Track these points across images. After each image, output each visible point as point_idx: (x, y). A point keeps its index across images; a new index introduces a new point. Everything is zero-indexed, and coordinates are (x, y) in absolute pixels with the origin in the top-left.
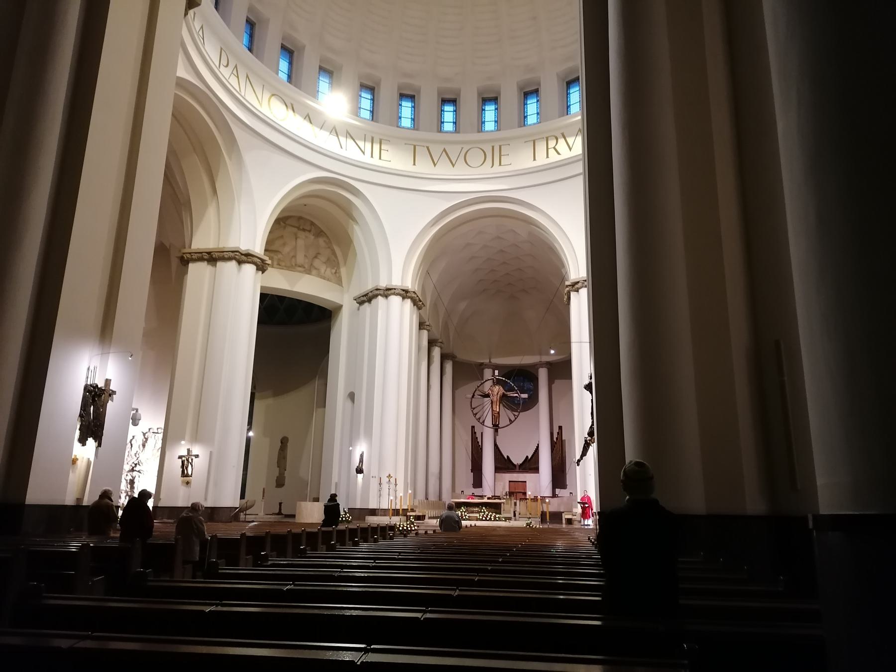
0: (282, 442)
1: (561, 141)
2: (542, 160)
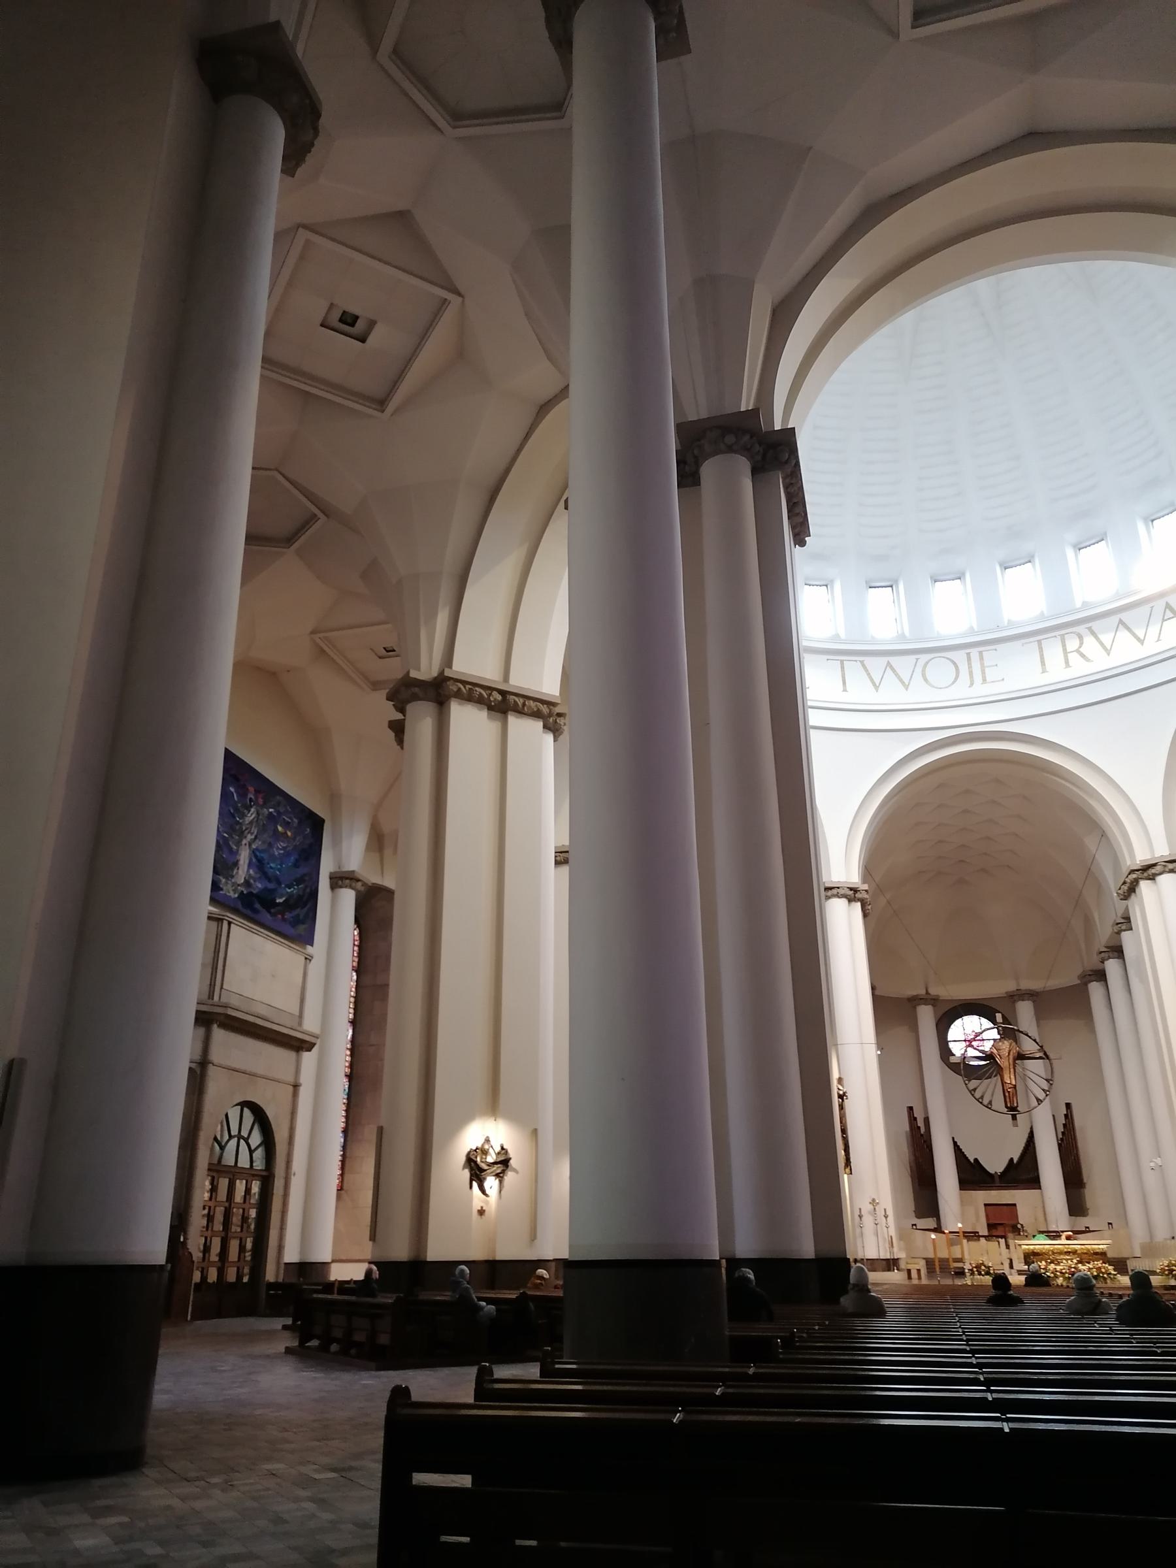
1: (1089, 640)
2: (1057, 673)
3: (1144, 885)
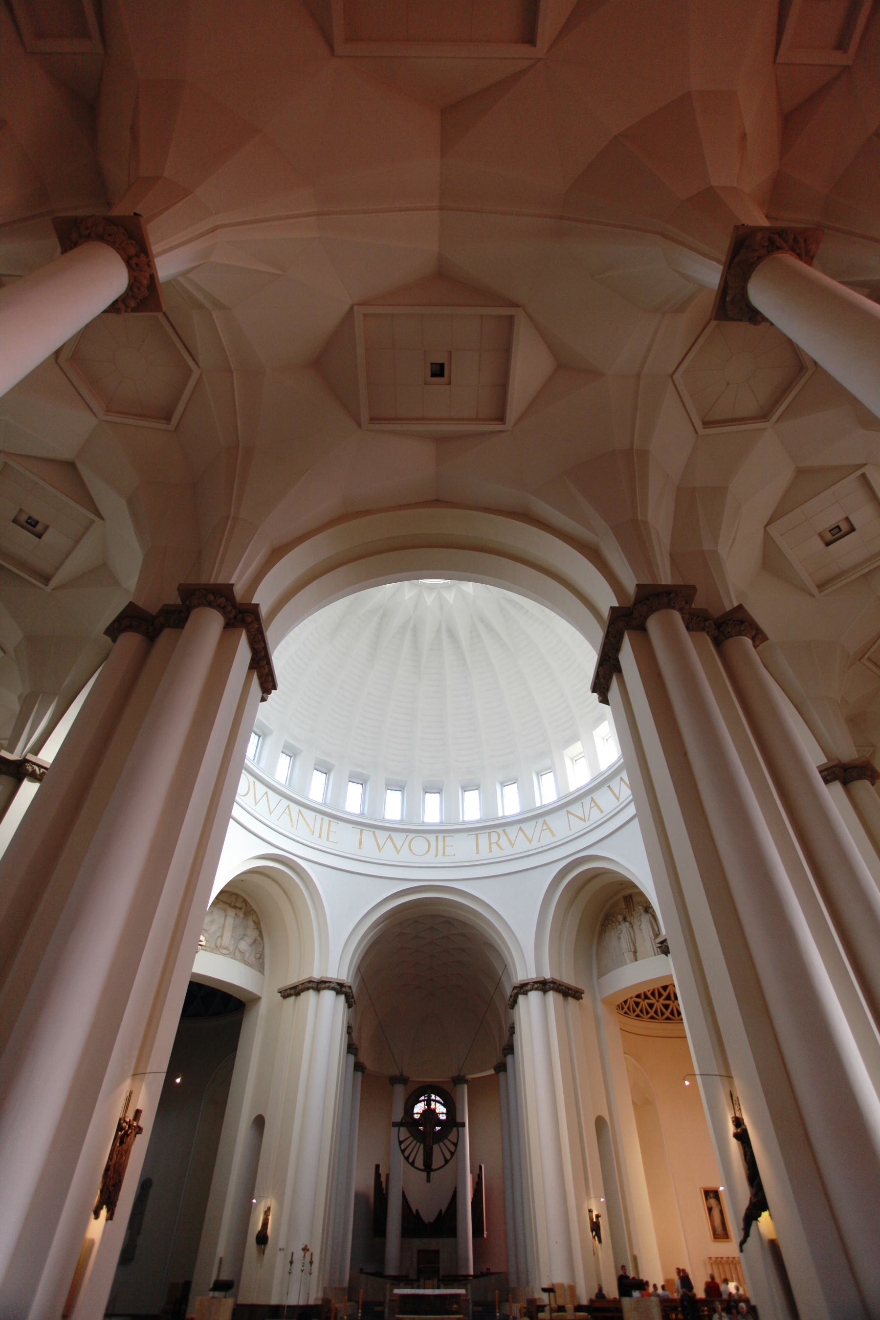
1: (503, 837)
3: (521, 999)
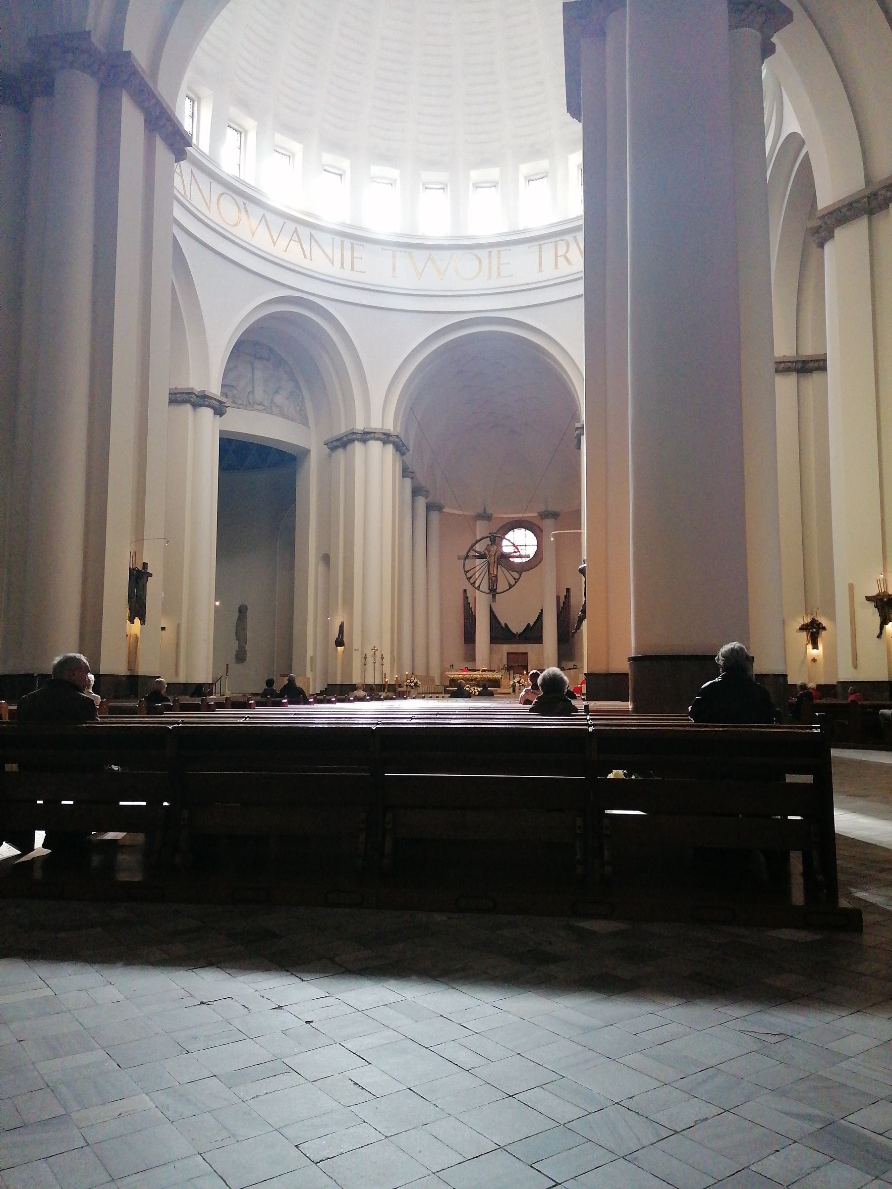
0: (240, 611)
